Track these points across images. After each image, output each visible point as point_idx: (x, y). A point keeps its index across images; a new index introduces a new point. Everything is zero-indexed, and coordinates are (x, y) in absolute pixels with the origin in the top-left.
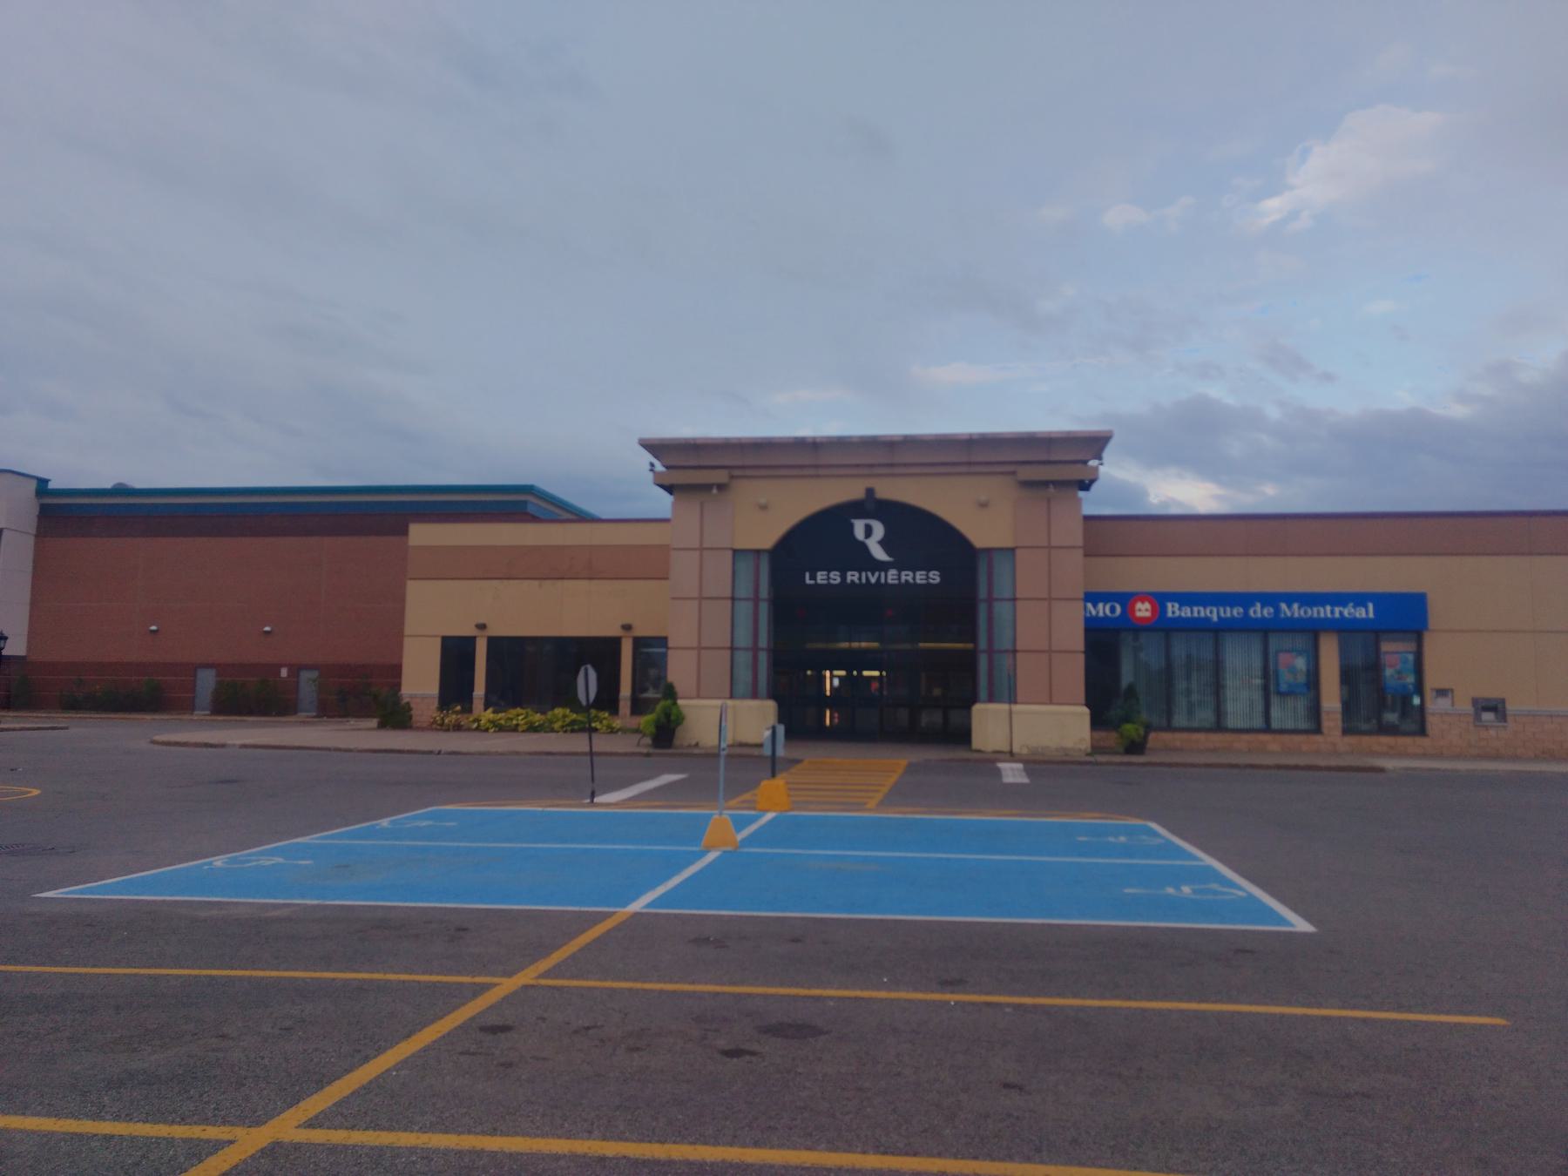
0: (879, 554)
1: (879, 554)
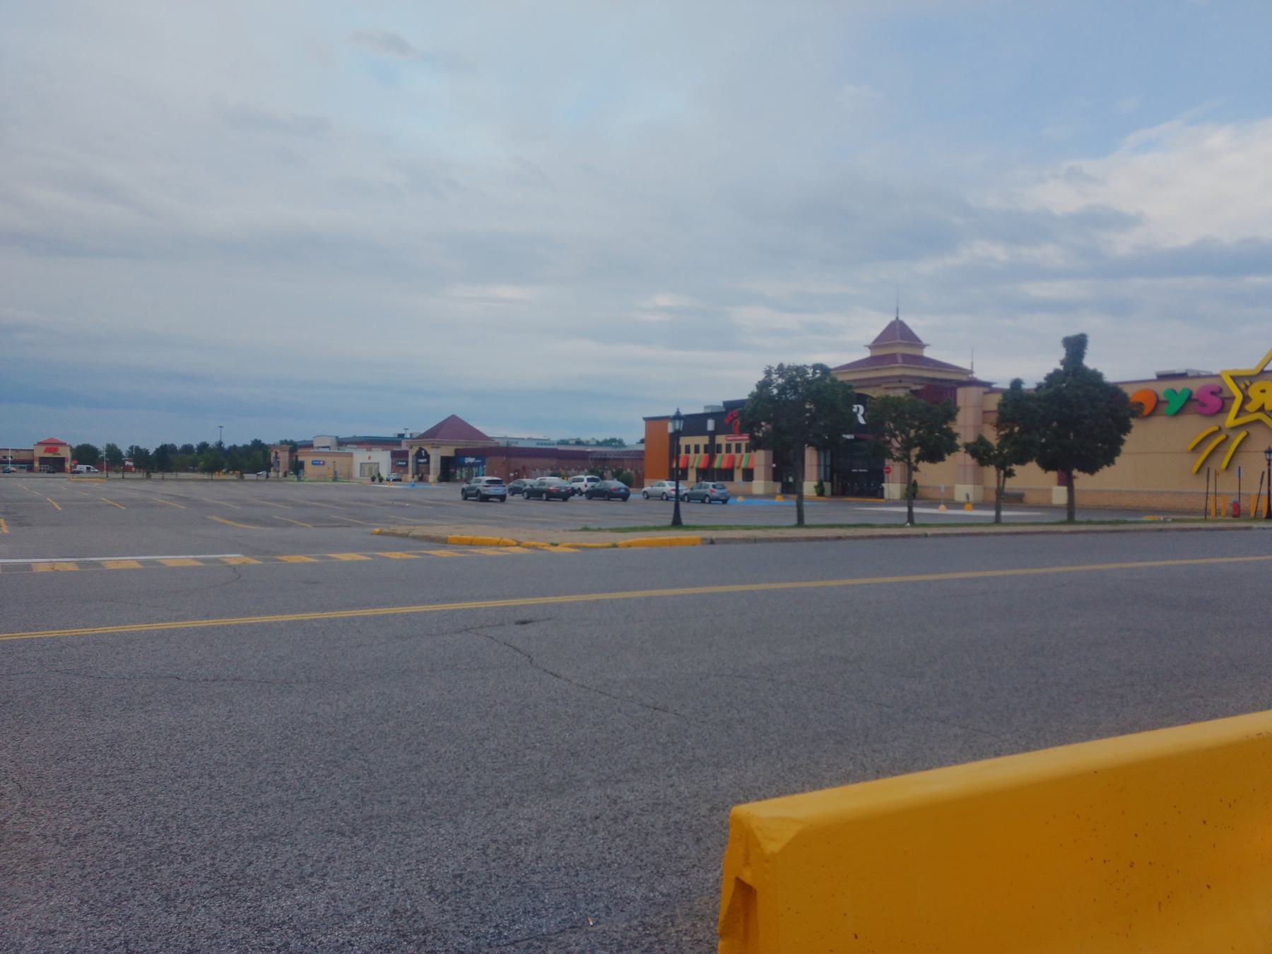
0: (862, 421)
1: (862, 421)
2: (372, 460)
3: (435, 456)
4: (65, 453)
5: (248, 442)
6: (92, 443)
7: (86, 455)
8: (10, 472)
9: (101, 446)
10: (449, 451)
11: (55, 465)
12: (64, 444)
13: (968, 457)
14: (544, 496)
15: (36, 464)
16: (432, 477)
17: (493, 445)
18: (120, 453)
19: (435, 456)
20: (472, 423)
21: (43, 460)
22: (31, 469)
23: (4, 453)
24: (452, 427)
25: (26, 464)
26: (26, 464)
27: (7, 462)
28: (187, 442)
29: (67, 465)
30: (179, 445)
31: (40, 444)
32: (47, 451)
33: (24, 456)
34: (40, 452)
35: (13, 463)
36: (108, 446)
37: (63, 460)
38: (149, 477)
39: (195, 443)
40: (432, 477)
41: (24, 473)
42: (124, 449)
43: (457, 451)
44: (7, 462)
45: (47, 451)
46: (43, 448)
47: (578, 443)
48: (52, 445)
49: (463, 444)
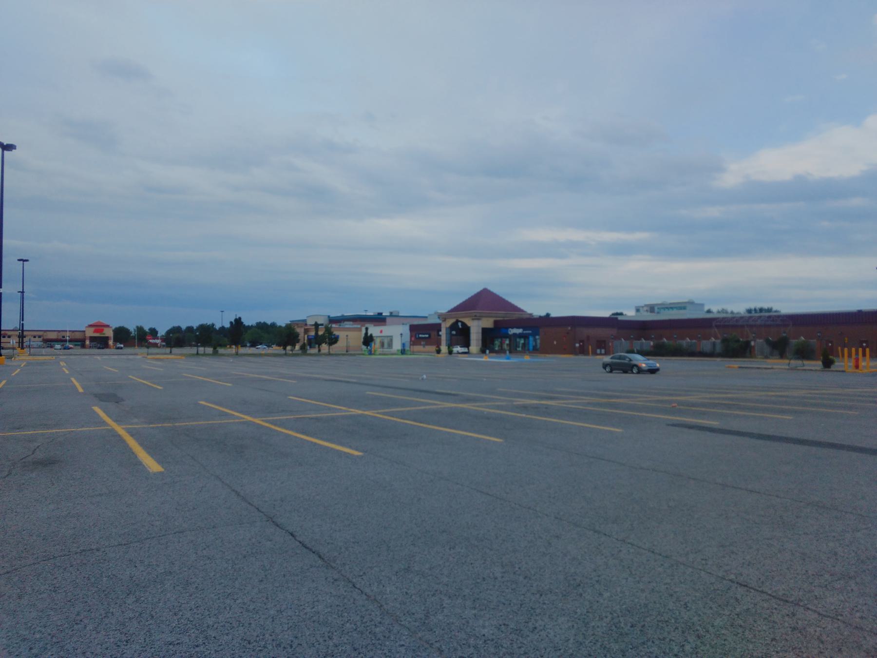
2: (383, 334)
3: (476, 328)
4: (109, 333)
5: (543, 314)
6: (127, 326)
7: (123, 336)
8: (69, 348)
9: (132, 328)
10: (488, 323)
11: (101, 342)
12: (108, 326)
13: (408, 332)
14: (635, 370)
15: (88, 342)
16: (475, 347)
17: (525, 316)
18: (157, 332)
19: (476, 328)
20: (504, 297)
21: (92, 339)
22: (83, 346)
23: (63, 334)
24: (483, 301)
25: (80, 342)
26: (80, 342)
27: (66, 341)
28: (189, 325)
29: (111, 342)
30: (184, 327)
31: (91, 326)
32: (95, 331)
33: (78, 336)
34: (90, 333)
35: (71, 341)
36: (137, 327)
37: (107, 338)
38: (215, 353)
39: (195, 325)
40: (475, 347)
41: (79, 350)
42: (146, 329)
43: (496, 322)
44: (66, 341)
45: (95, 331)
46: (93, 329)
47: (761, 310)
48: (99, 327)
49: (501, 315)
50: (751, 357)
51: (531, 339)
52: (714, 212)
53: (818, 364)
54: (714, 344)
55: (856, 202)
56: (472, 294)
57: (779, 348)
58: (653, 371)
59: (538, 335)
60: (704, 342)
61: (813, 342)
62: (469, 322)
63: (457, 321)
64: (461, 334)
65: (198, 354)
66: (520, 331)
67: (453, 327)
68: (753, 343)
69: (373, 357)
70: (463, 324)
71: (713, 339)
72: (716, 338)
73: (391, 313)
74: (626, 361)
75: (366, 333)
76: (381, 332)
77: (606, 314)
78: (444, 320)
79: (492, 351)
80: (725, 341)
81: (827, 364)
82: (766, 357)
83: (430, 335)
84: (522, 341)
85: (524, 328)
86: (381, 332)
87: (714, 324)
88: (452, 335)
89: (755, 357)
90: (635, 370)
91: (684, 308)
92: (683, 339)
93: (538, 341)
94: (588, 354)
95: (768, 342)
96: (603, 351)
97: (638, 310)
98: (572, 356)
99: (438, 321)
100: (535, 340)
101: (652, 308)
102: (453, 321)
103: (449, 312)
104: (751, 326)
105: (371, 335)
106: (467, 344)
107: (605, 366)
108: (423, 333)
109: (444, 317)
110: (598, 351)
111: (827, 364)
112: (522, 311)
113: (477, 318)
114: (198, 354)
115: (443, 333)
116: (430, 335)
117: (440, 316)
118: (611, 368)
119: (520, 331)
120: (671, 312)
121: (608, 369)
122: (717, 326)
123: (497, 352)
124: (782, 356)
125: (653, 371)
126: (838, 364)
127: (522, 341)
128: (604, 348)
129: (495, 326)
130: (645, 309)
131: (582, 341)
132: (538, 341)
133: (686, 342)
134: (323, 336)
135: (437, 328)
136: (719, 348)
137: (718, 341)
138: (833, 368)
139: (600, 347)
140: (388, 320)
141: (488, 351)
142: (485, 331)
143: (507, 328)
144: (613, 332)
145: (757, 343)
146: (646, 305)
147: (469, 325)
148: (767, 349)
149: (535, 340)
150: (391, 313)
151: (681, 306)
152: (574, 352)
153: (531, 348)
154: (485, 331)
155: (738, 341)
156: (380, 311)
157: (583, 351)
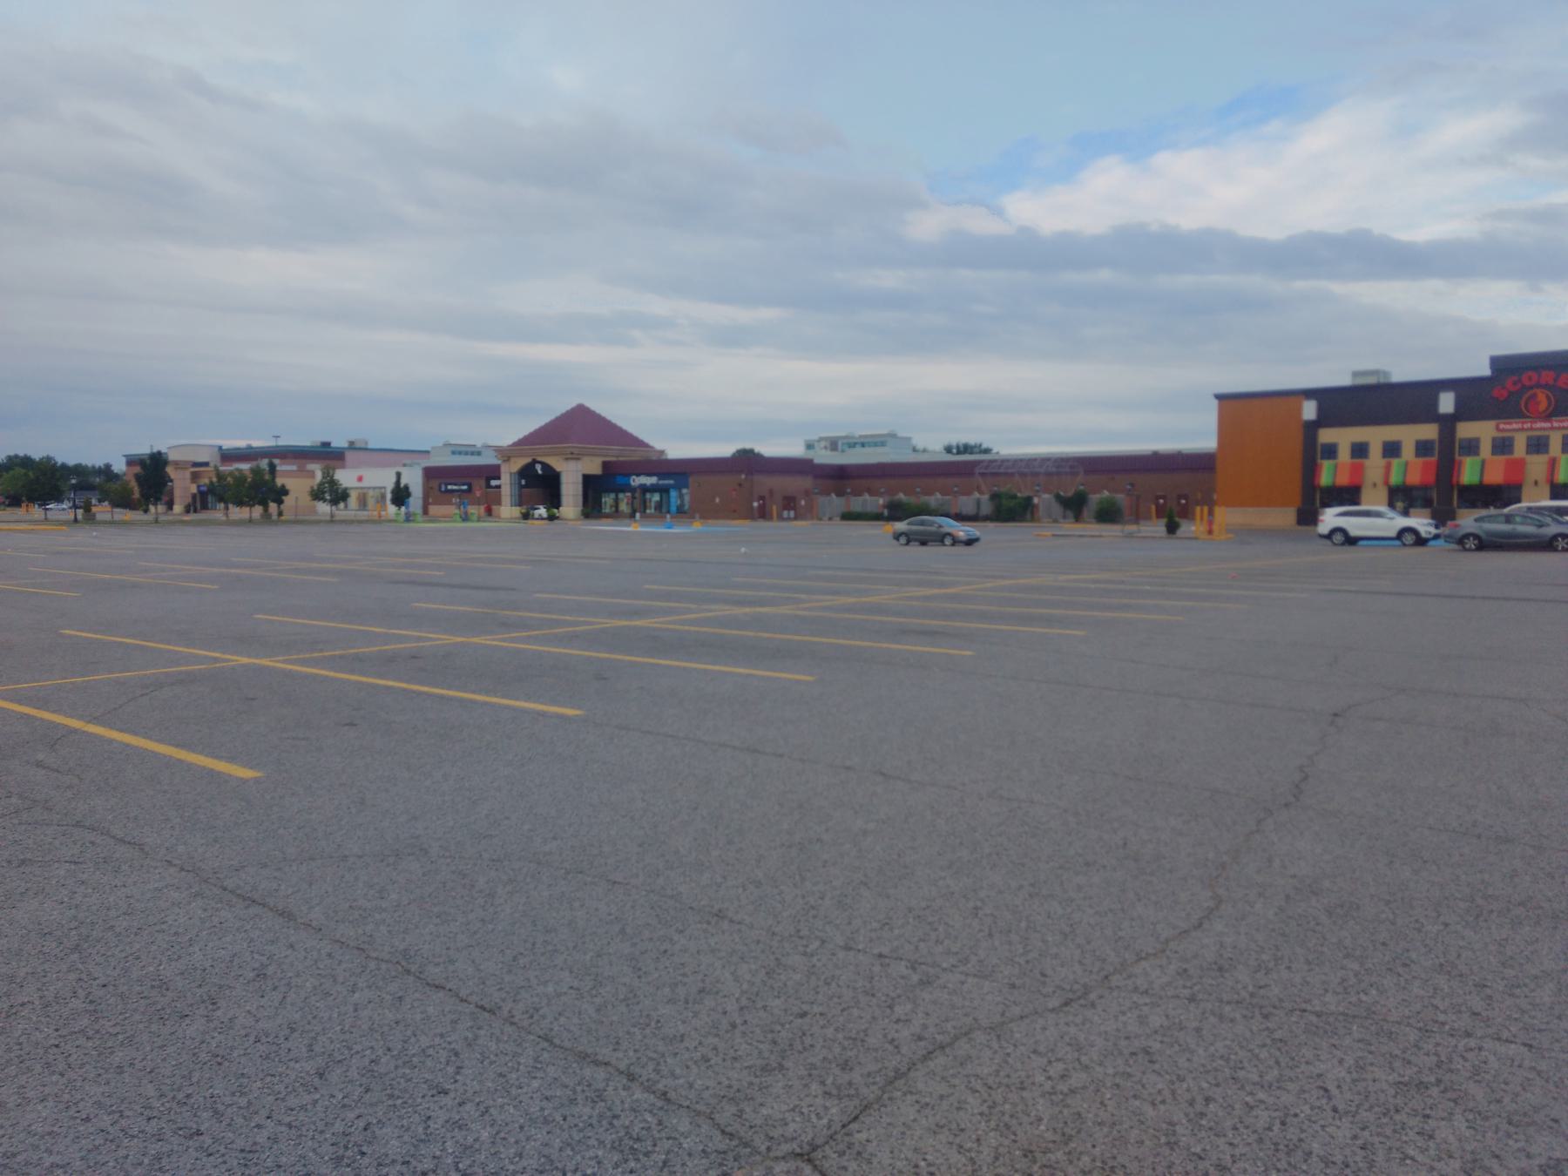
2: (364, 484)
10: (594, 467)
16: (571, 503)
43: (605, 465)
49: (615, 453)
50: (1033, 520)
51: (673, 494)
52: (889, 280)
53: (1159, 527)
54: (978, 502)
55: (1105, 275)
56: (569, 407)
57: (1074, 506)
58: (970, 542)
59: (687, 486)
60: (963, 499)
61: (1120, 497)
62: (557, 464)
63: (535, 462)
64: (541, 486)
65: (76, 520)
66: (650, 481)
67: (526, 473)
68: (1036, 500)
69: (412, 525)
70: (545, 466)
71: (977, 495)
72: (981, 492)
73: (352, 443)
74: (933, 529)
75: (398, 482)
76: (360, 479)
77: (725, 450)
78: (507, 459)
79: (644, 515)
80: (995, 497)
81: (1172, 528)
82: (1056, 521)
83: (470, 485)
84: (656, 497)
85: (661, 476)
86: (360, 479)
87: (977, 471)
88: (522, 487)
89: (1039, 520)
90: (948, 541)
91: (883, 444)
92: (930, 493)
93: (687, 499)
94: (771, 519)
95: (1058, 497)
96: (792, 514)
97: (809, 446)
98: (747, 522)
99: (495, 461)
100: (681, 496)
101: (833, 444)
102: (529, 460)
103: (515, 444)
104: (1023, 475)
105: (406, 487)
106: (554, 500)
107: (897, 536)
108: (459, 483)
109: (506, 454)
110: (785, 514)
111: (1172, 528)
112: (647, 445)
113: (574, 457)
114: (76, 520)
115: (506, 483)
116: (470, 485)
117: (499, 450)
118: (908, 538)
119: (650, 481)
120: (867, 450)
121: (903, 540)
122: (983, 474)
123: (607, 516)
124: (1078, 518)
125: (970, 542)
126: (1186, 528)
127: (656, 497)
128: (794, 508)
129: (592, 473)
130: (823, 444)
131: (762, 498)
132: (687, 499)
133: (934, 500)
134: (247, 485)
135: (492, 473)
136: (987, 508)
137: (986, 497)
138: (1179, 533)
139: (787, 507)
140: (349, 456)
141: (638, 515)
142: (588, 480)
143: (629, 475)
144: (807, 482)
145: (1043, 500)
146: (821, 439)
147: (558, 469)
148: (1057, 509)
149: (681, 496)
150: (352, 443)
151: (878, 441)
152: (750, 515)
153: (673, 509)
154: (588, 480)
155: (1014, 497)
156: (326, 439)
157: (763, 514)
